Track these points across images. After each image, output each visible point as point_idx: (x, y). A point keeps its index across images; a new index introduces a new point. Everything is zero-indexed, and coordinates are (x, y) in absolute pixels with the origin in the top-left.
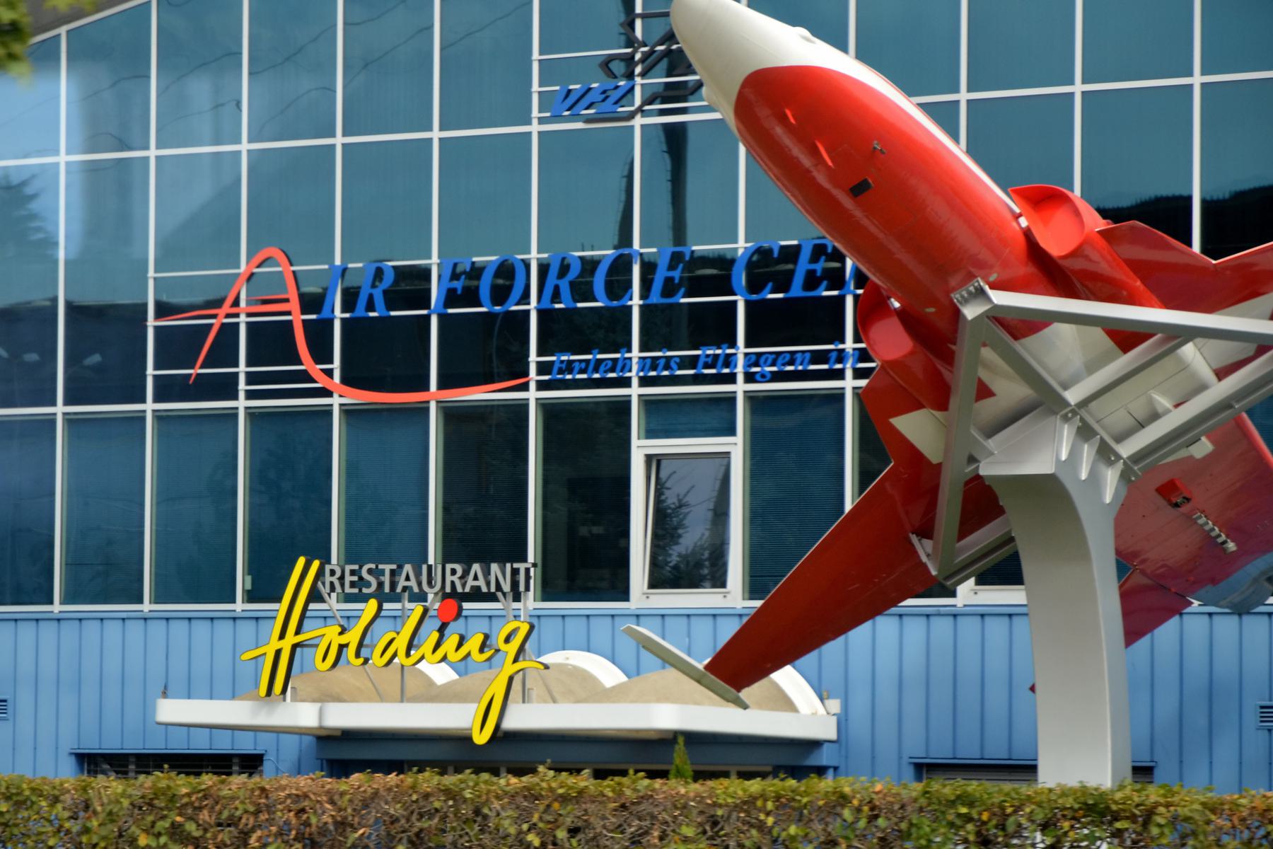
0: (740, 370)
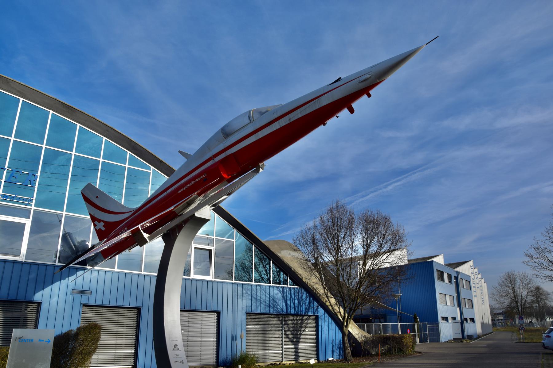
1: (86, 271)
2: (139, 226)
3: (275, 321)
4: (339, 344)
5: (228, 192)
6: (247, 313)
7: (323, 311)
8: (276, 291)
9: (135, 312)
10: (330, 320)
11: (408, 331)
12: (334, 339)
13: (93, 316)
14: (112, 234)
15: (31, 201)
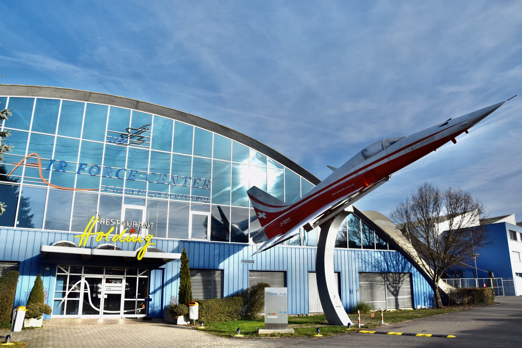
3: (379, 278)
4: (430, 295)
6: (360, 273)
7: (415, 270)
8: (379, 255)
9: (282, 274)
10: (421, 276)
11: (485, 285)
12: (425, 291)
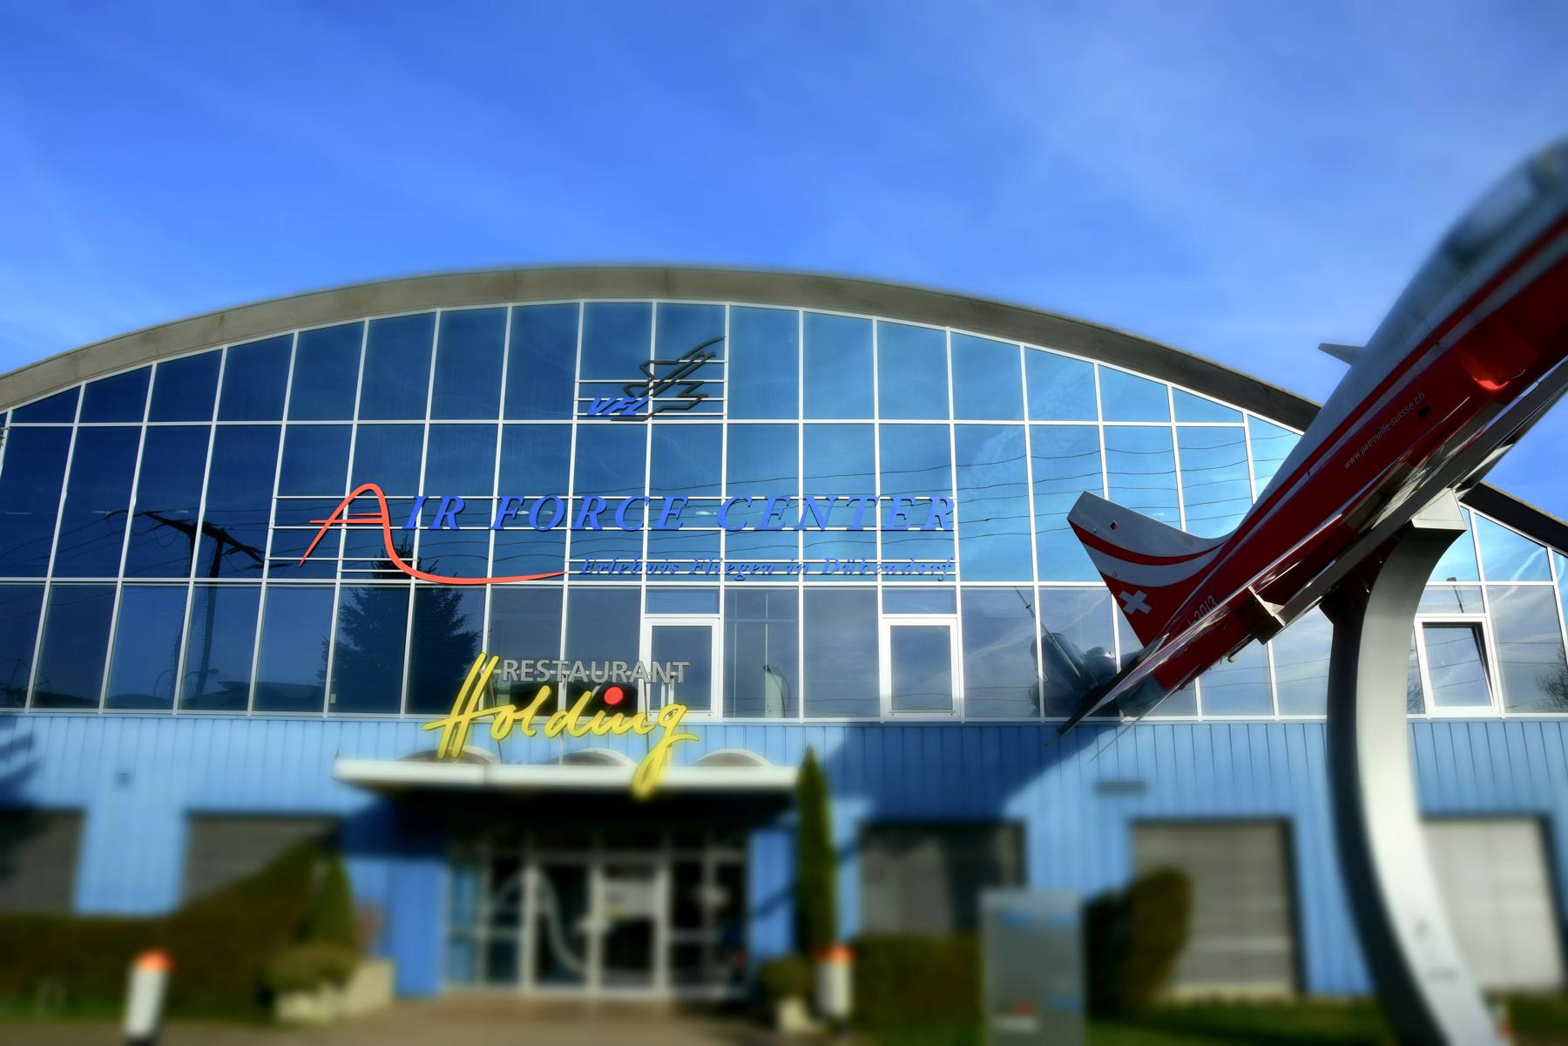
0: (722, 571)
1: (1120, 729)
2: (1249, 586)
5: (1509, 434)
13: (1162, 851)
14: (1173, 619)
15: (951, 566)
